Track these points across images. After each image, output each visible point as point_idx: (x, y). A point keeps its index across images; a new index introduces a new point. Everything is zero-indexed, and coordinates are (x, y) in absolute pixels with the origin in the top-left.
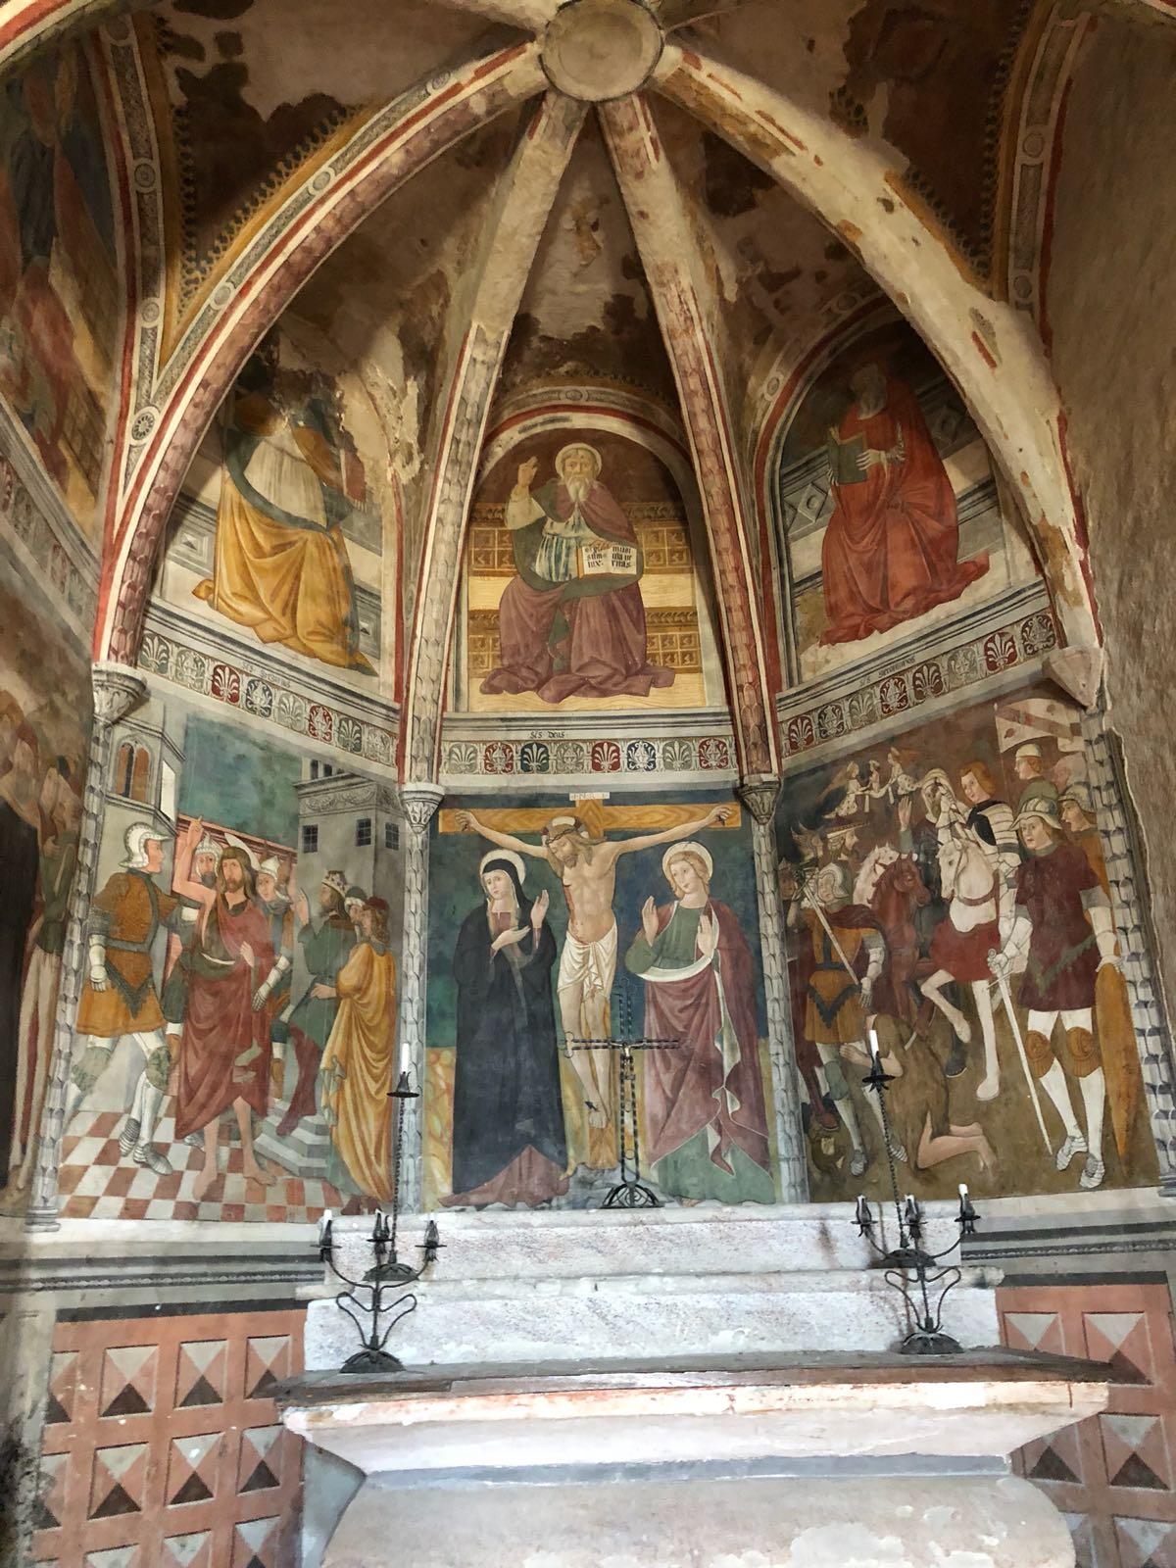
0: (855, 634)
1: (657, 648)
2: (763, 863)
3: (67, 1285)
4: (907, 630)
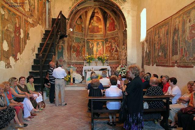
2: (105, 43)
4: (112, 32)
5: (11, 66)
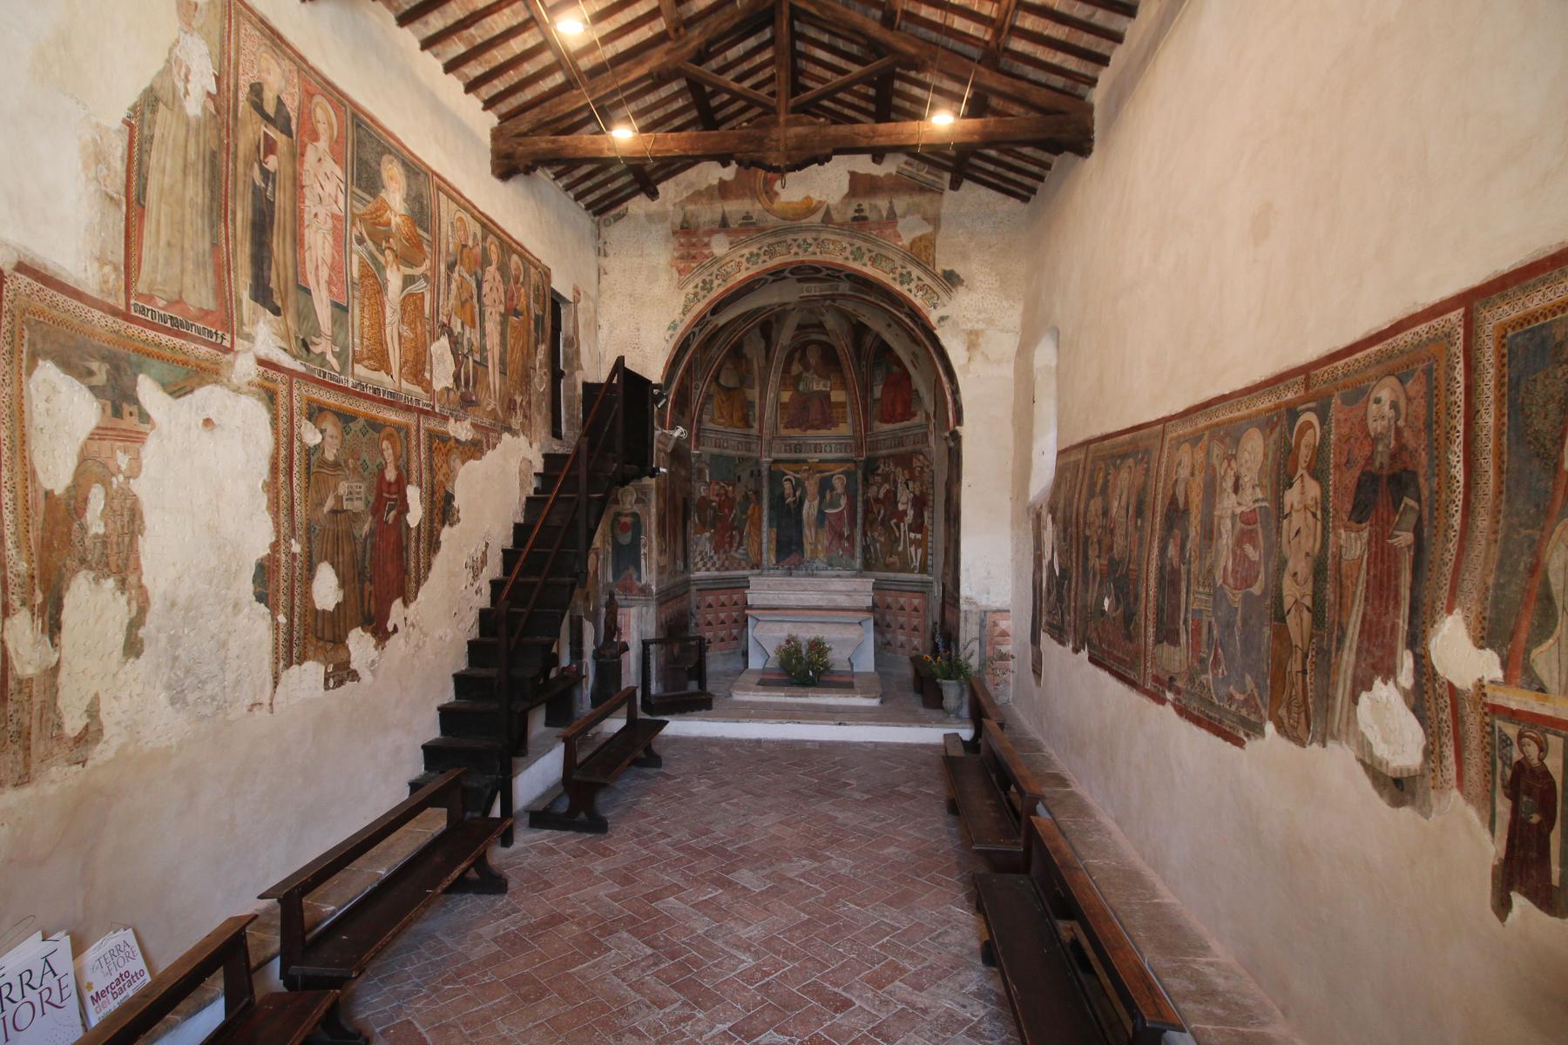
0: (887, 422)
4: (898, 425)
5: (355, 671)
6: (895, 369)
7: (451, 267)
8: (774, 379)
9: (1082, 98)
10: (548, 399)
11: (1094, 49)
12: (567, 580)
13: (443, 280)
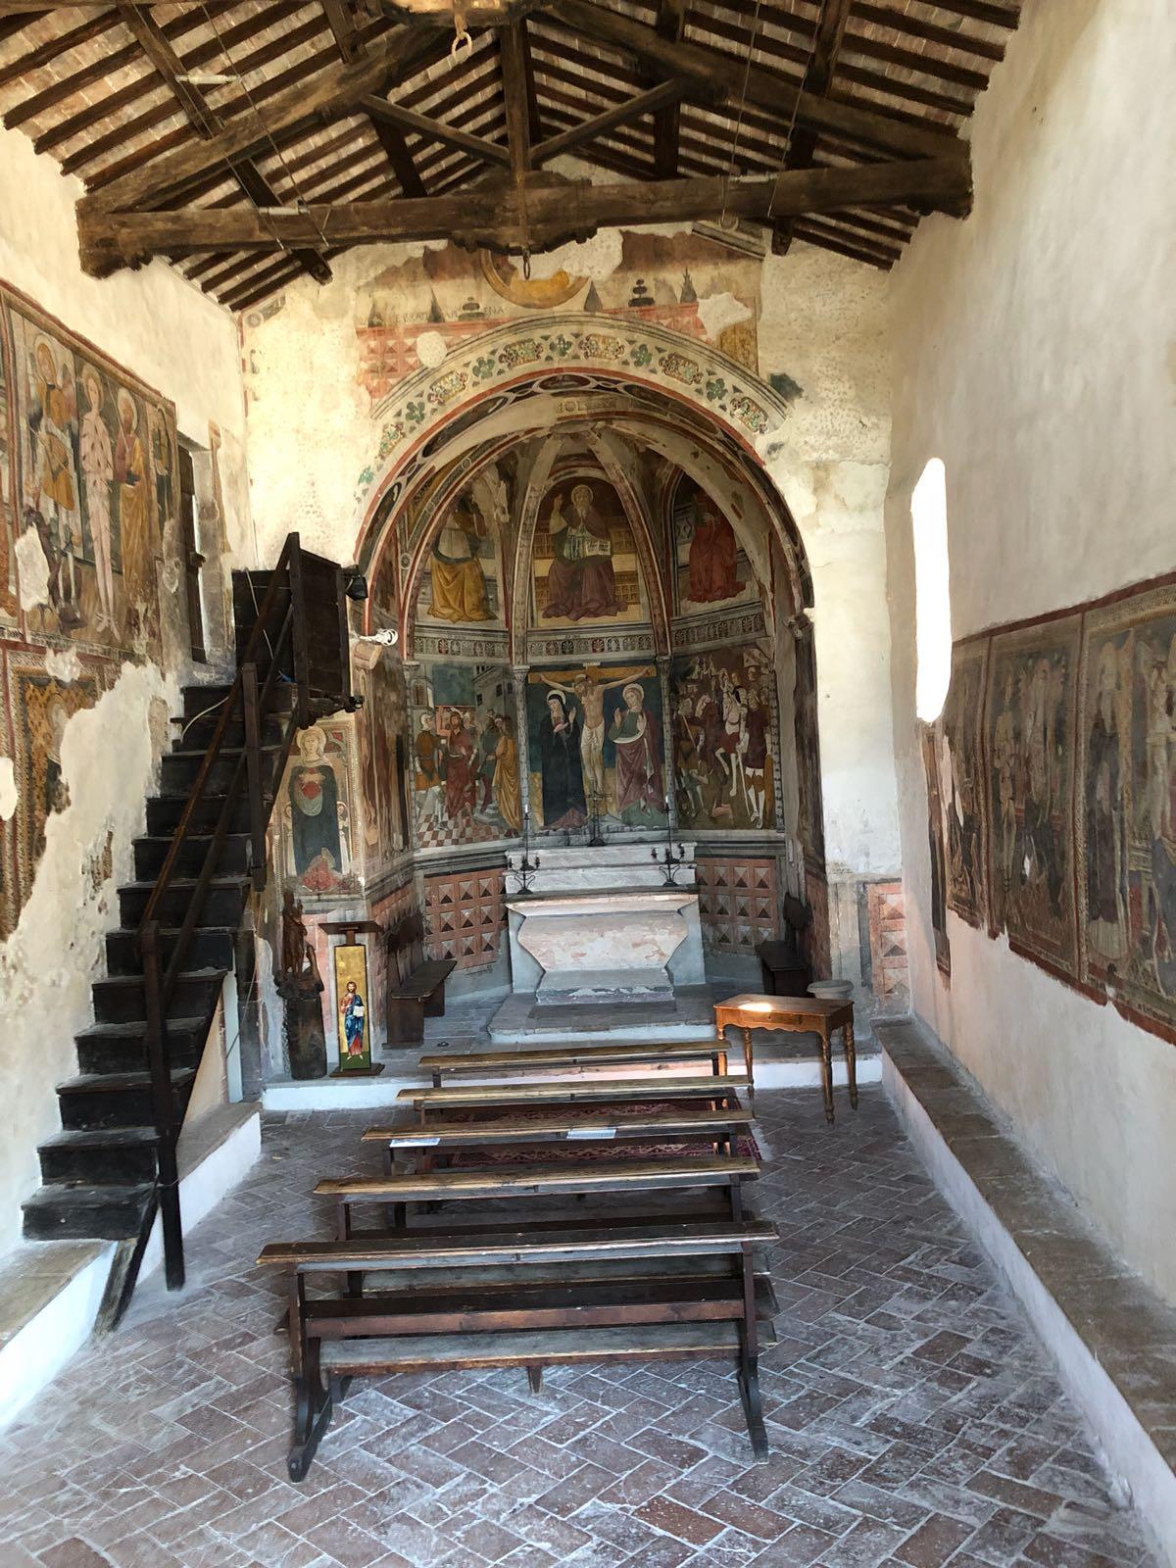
0: (701, 599)
1: (620, 593)
2: (665, 692)
3: (425, 867)
4: (718, 604)
6: (708, 517)
7: (34, 422)
8: (522, 546)
9: (952, 131)
10: (183, 602)
11: (964, 65)
12: (239, 879)
13: (25, 443)
